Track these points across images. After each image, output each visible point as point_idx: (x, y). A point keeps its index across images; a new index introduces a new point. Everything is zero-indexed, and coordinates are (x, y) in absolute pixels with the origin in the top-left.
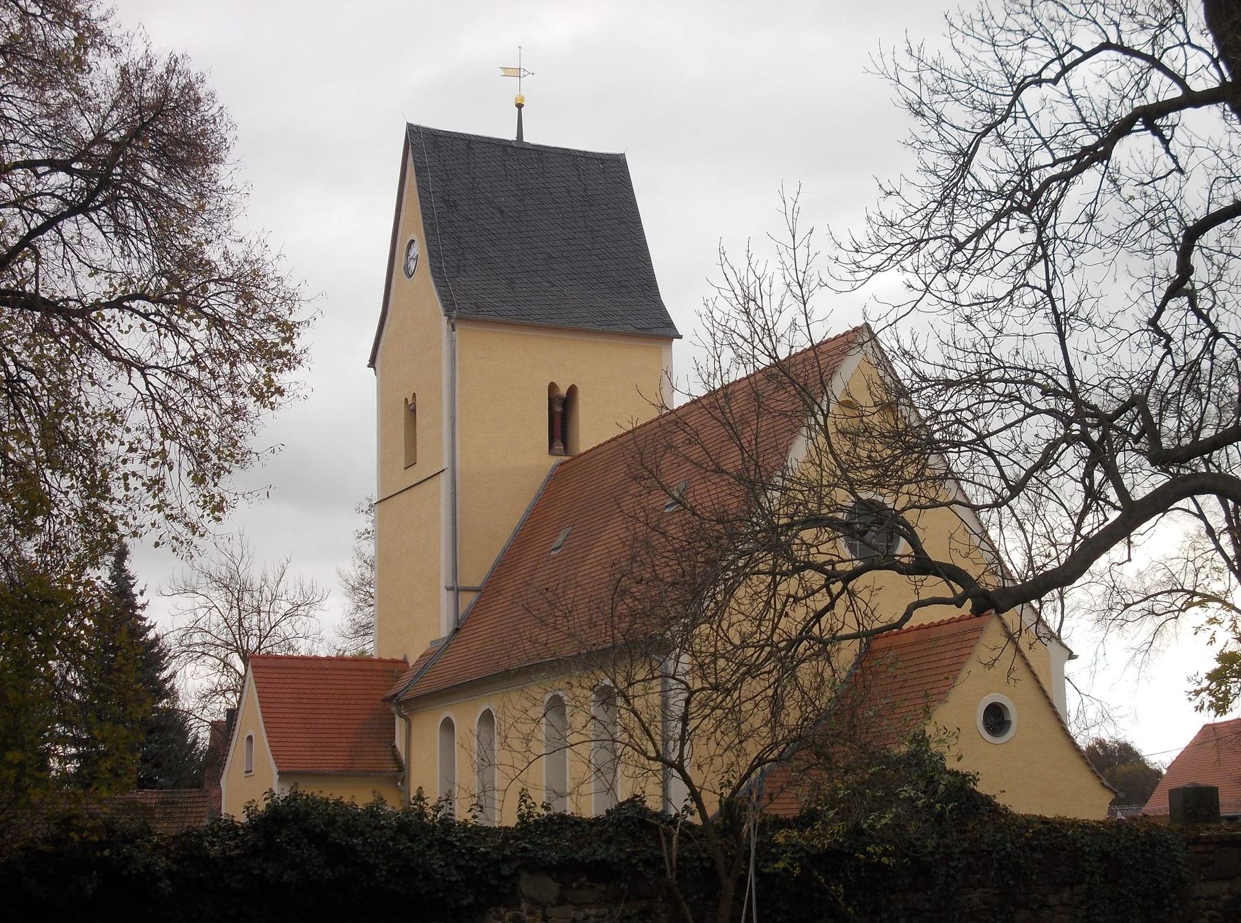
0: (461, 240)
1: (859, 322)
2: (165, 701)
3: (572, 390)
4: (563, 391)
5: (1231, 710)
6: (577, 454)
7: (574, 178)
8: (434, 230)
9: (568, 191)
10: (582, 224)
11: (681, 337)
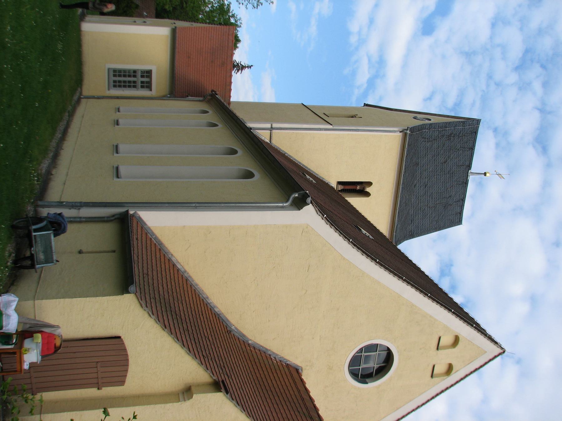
0: (435, 141)
1: (14, 311)
3: (368, 194)
4: (368, 190)
7: (455, 200)
9: (450, 196)
10: (437, 203)
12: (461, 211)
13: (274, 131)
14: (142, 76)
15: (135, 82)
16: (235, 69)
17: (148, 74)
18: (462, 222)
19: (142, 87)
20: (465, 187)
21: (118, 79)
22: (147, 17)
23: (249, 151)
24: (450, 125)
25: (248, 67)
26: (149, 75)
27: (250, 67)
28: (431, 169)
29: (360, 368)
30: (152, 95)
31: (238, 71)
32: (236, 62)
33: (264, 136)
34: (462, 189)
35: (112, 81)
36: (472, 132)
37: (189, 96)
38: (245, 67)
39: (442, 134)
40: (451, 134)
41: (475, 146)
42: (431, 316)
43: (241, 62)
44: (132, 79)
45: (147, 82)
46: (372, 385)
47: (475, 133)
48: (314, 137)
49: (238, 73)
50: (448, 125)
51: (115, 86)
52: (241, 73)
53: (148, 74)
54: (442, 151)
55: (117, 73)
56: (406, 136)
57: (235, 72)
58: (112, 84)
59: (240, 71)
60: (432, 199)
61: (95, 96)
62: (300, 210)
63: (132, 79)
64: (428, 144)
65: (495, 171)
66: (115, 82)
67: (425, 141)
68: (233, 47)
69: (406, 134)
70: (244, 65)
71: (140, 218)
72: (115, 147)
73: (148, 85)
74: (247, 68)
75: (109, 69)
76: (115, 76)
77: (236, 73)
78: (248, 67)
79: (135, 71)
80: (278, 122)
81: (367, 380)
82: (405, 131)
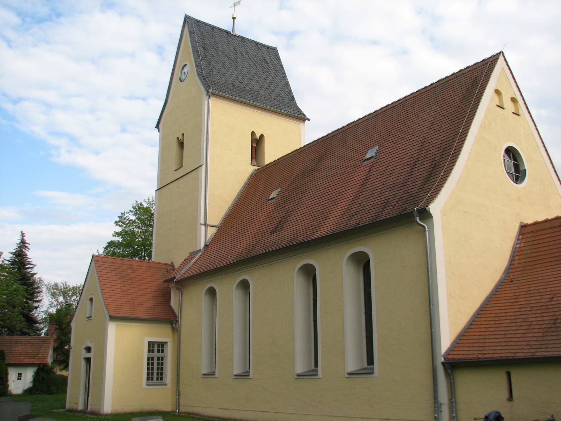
0: (211, 64)
2: (16, 266)
3: (262, 136)
4: (258, 136)
5: (77, 285)
6: (262, 166)
8: (199, 57)
9: (255, 56)
10: (262, 69)
11: (309, 120)
12: (266, 47)
13: (208, 222)
14: (153, 351)
15: (158, 359)
16: (24, 250)
17: (151, 345)
18: (275, 47)
19: (162, 351)
20: (245, 39)
21: (155, 376)
22: (69, 345)
23: (308, 253)
24: (195, 47)
25: (23, 236)
26: (151, 345)
27: (23, 234)
28: (235, 72)
29: (515, 175)
30: (171, 342)
31: (26, 247)
32: (16, 248)
33: (212, 231)
34: (248, 43)
35: (158, 381)
36: (197, 25)
37: (169, 305)
38: (23, 239)
39: (204, 56)
40: (203, 47)
41: (210, 24)
42: (486, 112)
43: (17, 244)
44: (155, 361)
45: (159, 347)
46: (527, 165)
47: (198, 23)
48: (213, 184)
49: (29, 247)
50: (196, 49)
51: (162, 379)
52: (29, 244)
53: (151, 345)
54: (218, 58)
55: (150, 377)
56: (215, 93)
57: (27, 251)
58: (160, 381)
59: (27, 245)
60: (260, 74)
61: (177, 398)
62: (432, 217)
63: (155, 361)
64: (215, 72)
65: (230, 8)
66: (158, 379)
67: (213, 74)
68: (119, 258)
69: (213, 94)
70: (20, 241)
71: (446, 352)
72: (299, 377)
73: (162, 346)
74: (24, 238)
75: (147, 385)
76: (152, 379)
77: (29, 249)
78: (23, 236)
79: (149, 359)
80: (197, 218)
81: (521, 169)
82: (210, 93)
